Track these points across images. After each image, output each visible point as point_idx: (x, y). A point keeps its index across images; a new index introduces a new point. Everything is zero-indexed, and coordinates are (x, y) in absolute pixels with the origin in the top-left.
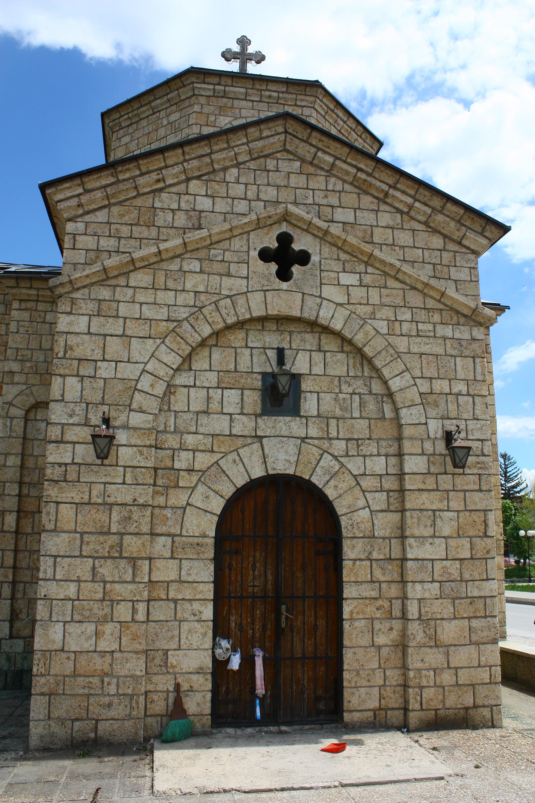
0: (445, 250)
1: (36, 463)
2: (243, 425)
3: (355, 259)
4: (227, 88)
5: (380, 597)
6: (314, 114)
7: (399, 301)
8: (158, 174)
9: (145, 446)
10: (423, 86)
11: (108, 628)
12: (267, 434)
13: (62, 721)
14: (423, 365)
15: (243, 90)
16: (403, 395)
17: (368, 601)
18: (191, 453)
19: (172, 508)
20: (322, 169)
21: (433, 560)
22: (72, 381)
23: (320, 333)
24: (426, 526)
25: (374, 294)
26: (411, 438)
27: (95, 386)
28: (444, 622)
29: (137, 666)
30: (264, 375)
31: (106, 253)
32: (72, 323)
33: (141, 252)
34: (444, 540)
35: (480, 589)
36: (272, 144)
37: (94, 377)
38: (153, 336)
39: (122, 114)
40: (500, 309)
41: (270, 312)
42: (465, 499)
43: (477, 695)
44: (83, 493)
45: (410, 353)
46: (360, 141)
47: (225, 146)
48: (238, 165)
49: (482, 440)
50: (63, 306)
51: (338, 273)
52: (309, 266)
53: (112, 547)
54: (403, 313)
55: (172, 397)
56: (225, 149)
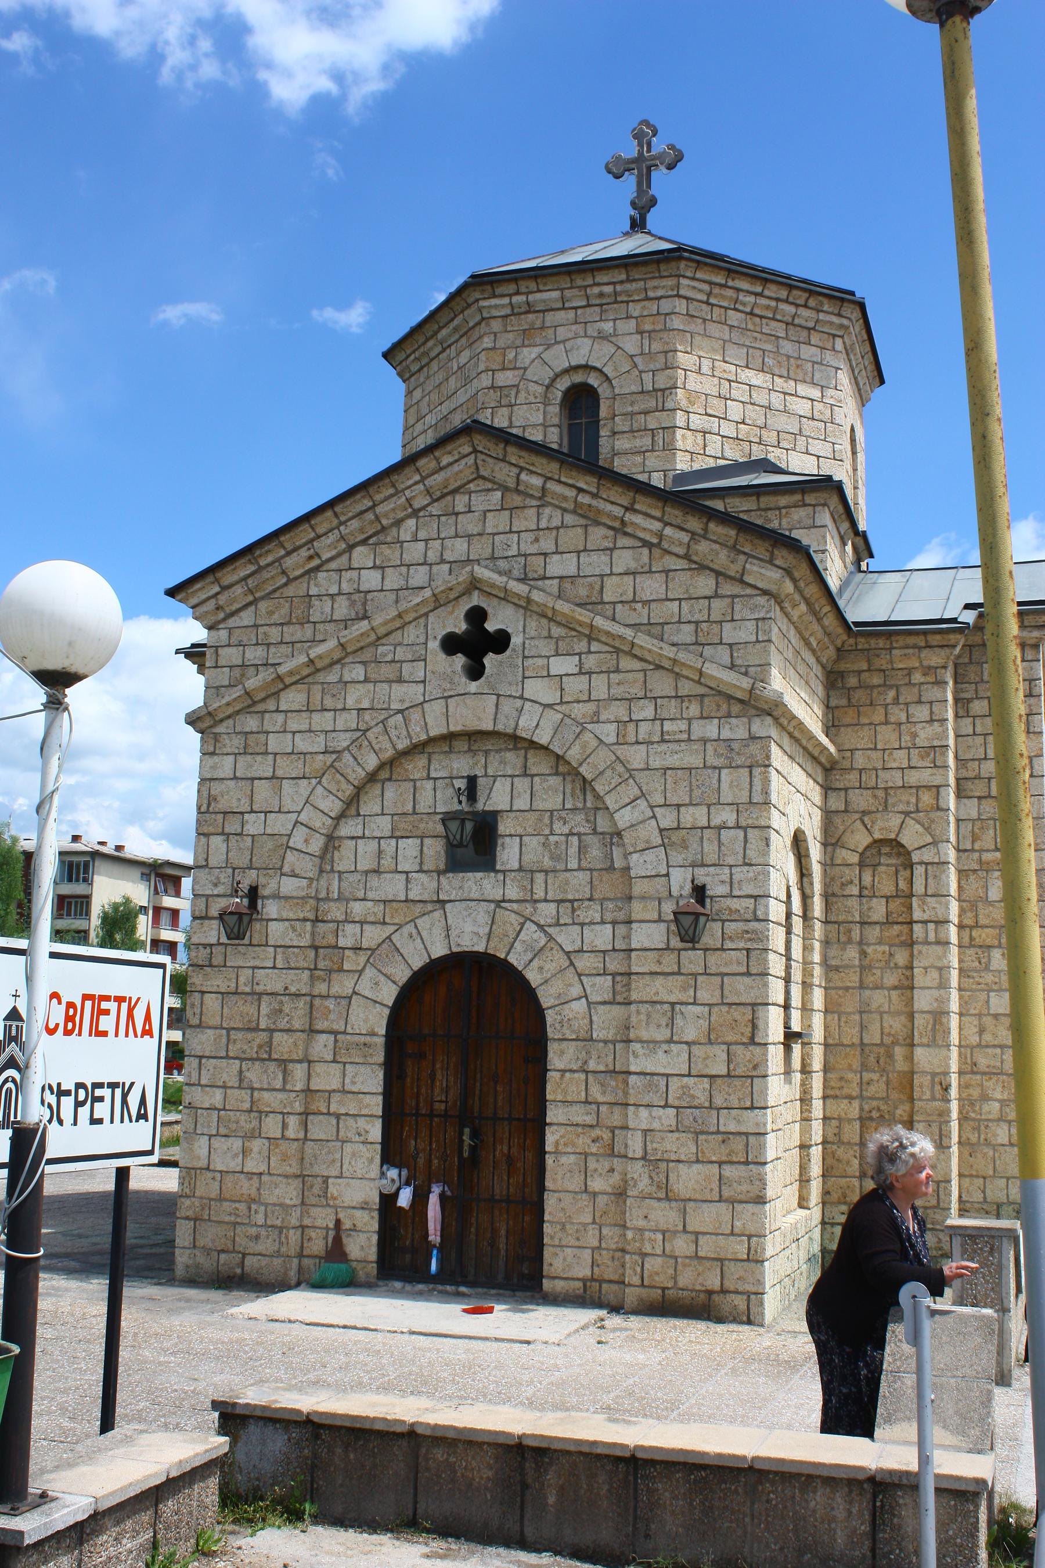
0: (716, 596)
2: (423, 887)
3: (574, 633)
4: (531, 297)
5: (597, 1125)
11: (256, 1145)
13: (207, 1251)
15: (556, 294)
17: (580, 1130)
20: (532, 496)
21: (667, 1075)
23: (526, 749)
24: (659, 1026)
28: (681, 1165)
29: (288, 1193)
30: (447, 818)
31: (252, 669)
34: (685, 1047)
35: (739, 1121)
37: (241, 834)
43: (727, 1275)
44: (230, 980)
47: (391, 491)
48: (415, 513)
49: (756, 897)
51: (548, 657)
52: (508, 652)
53: (260, 1047)
56: (392, 496)
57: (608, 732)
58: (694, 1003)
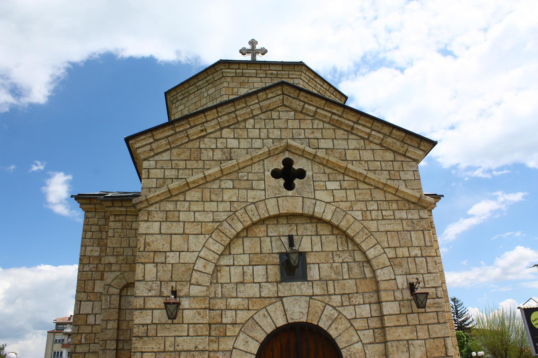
0: (395, 161)
1: (128, 326)
2: (269, 290)
3: (336, 172)
4: (244, 71)
6: (301, 82)
7: (368, 197)
8: (202, 126)
9: (202, 309)
10: (373, 62)
12: (286, 295)
14: (389, 239)
15: (254, 71)
16: (377, 261)
18: (234, 311)
19: (223, 351)
20: (309, 115)
22: (150, 267)
23: (316, 223)
24: (403, 352)
25: (351, 193)
26: (386, 290)
27: (166, 269)
30: (281, 254)
31: (170, 180)
32: (149, 227)
33: (193, 178)
36: (274, 102)
37: (165, 263)
38: (203, 233)
39: (178, 92)
40: (437, 197)
41: (281, 212)
42: (428, 330)
44: (160, 344)
45: (379, 231)
46: (333, 97)
47: (244, 105)
48: (253, 117)
49: (436, 287)
50: (143, 216)
51: (325, 182)
52: (305, 179)
54: (372, 205)
55: (219, 273)
56: (244, 107)
57: (358, 215)
58: (417, 339)
